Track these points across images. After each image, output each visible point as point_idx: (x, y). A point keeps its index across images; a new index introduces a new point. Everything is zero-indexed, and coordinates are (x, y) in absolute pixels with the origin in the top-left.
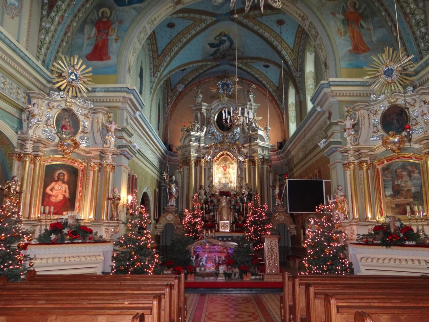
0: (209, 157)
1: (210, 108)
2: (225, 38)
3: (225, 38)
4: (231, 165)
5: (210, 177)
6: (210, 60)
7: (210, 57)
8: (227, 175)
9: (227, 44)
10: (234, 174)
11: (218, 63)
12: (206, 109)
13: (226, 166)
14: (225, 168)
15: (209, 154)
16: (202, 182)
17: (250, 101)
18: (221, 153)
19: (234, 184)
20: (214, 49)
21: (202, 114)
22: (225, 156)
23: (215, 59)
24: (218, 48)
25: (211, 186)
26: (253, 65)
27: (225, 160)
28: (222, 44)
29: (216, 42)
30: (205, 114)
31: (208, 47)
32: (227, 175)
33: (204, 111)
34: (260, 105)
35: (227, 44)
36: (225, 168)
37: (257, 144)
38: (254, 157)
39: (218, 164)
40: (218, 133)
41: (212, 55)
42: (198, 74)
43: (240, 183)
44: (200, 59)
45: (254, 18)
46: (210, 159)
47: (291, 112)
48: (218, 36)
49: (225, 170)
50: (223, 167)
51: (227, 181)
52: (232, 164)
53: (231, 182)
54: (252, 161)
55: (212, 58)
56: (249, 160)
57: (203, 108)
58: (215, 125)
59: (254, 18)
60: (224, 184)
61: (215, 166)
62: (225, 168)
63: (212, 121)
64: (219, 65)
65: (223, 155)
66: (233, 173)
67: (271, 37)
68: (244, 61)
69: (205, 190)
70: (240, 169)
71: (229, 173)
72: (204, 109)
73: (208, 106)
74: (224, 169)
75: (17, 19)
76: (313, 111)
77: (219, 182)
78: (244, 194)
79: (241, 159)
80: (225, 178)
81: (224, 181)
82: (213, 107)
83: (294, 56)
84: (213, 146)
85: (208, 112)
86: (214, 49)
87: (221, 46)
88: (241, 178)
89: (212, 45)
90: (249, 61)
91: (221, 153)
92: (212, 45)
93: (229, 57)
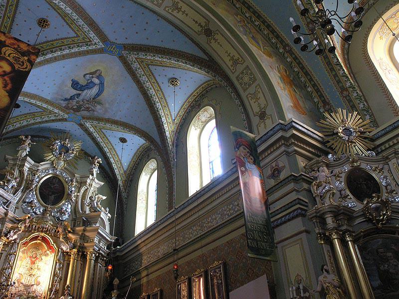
0: (16, 237)
1: (36, 168)
2: (96, 81)
3: (96, 81)
6: (59, 107)
7: (62, 102)
8: (34, 272)
9: (95, 90)
11: (66, 116)
12: (29, 168)
17: (93, 175)
18: (36, 234)
20: (75, 92)
21: (21, 173)
22: (39, 241)
23: (66, 109)
24: (80, 92)
26: (108, 133)
27: (37, 247)
28: (88, 88)
29: (83, 82)
30: (26, 174)
31: (69, 84)
32: (34, 272)
33: (26, 169)
34: (103, 183)
35: (95, 90)
37: (96, 230)
38: (85, 248)
39: (23, 252)
40: (38, 205)
41: (66, 99)
42: (32, 121)
44: (49, 98)
45: (148, 65)
46: (15, 240)
47: (141, 201)
48: (91, 74)
49: (33, 263)
51: (32, 281)
53: (38, 284)
54: (82, 255)
55: (64, 104)
56: (78, 251)
57: (26, 164)
58: (36, 194)
59: (148, 65)
60: (26, 286)
63: (34, 186)
64: (66, 120)
65: (36, 238)
67: (156, 97)
68: (101, 124)
70: (248, 194)
71: (39, 269)
72: (27, 167)
73: (34, 165)
76: (212, 186)
79: (65, 248)
82: (40, 168)
83: (173, 129)
84: (28, 221)
85: (30, 172)
86: (75, 92)
87: (85, 91)
89: (75, 85)
90: (108, 125)
91: (36, 234)
92: (75, 85)
93: (85, 113)
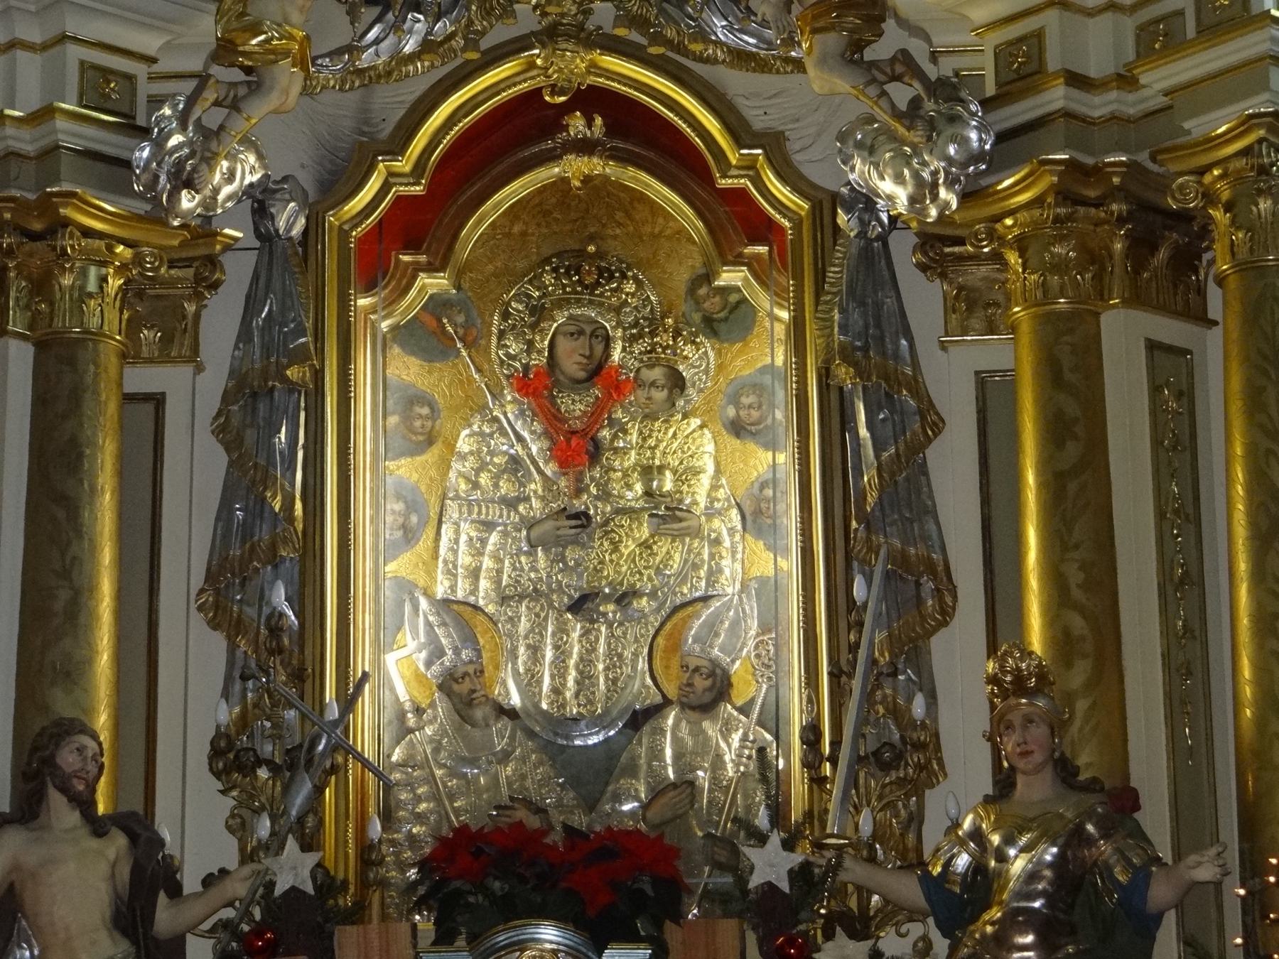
4: (697, 358)
5: (272, 581)
8: (625, 554)
10: (757, 518)
13: (597, 370)
14: (579, 415)
15: (280, 702)
16: (73, 673)
19: (774, 721)
25: (283, 728)
27: (581, 246)
32: (625, 554)
36: (575, 406)
39: (429, 336)
43: (879, 676)
50: (538, 387)
52: (726, 321)
53: (709, 692)
60: (546, 732)
61: (379, 377)
62: (579, 415)
66: (730, 502)
69: (136, 826)
71: (670, 515)
74: (552, 420)
75: (787, 133)
77: (462, 692)
78: (982, 882)
80: (581, 605)
81: (538, 669)
88: (876, 549)
